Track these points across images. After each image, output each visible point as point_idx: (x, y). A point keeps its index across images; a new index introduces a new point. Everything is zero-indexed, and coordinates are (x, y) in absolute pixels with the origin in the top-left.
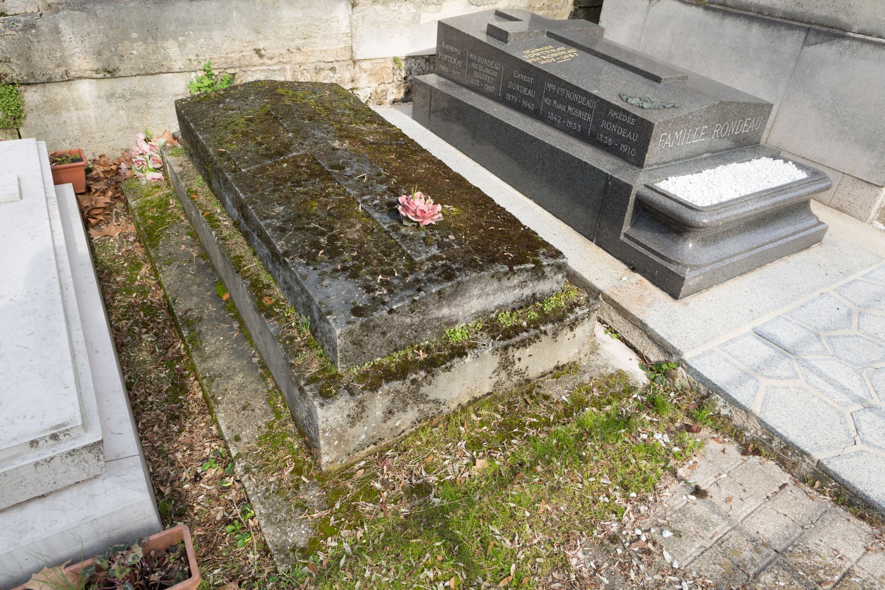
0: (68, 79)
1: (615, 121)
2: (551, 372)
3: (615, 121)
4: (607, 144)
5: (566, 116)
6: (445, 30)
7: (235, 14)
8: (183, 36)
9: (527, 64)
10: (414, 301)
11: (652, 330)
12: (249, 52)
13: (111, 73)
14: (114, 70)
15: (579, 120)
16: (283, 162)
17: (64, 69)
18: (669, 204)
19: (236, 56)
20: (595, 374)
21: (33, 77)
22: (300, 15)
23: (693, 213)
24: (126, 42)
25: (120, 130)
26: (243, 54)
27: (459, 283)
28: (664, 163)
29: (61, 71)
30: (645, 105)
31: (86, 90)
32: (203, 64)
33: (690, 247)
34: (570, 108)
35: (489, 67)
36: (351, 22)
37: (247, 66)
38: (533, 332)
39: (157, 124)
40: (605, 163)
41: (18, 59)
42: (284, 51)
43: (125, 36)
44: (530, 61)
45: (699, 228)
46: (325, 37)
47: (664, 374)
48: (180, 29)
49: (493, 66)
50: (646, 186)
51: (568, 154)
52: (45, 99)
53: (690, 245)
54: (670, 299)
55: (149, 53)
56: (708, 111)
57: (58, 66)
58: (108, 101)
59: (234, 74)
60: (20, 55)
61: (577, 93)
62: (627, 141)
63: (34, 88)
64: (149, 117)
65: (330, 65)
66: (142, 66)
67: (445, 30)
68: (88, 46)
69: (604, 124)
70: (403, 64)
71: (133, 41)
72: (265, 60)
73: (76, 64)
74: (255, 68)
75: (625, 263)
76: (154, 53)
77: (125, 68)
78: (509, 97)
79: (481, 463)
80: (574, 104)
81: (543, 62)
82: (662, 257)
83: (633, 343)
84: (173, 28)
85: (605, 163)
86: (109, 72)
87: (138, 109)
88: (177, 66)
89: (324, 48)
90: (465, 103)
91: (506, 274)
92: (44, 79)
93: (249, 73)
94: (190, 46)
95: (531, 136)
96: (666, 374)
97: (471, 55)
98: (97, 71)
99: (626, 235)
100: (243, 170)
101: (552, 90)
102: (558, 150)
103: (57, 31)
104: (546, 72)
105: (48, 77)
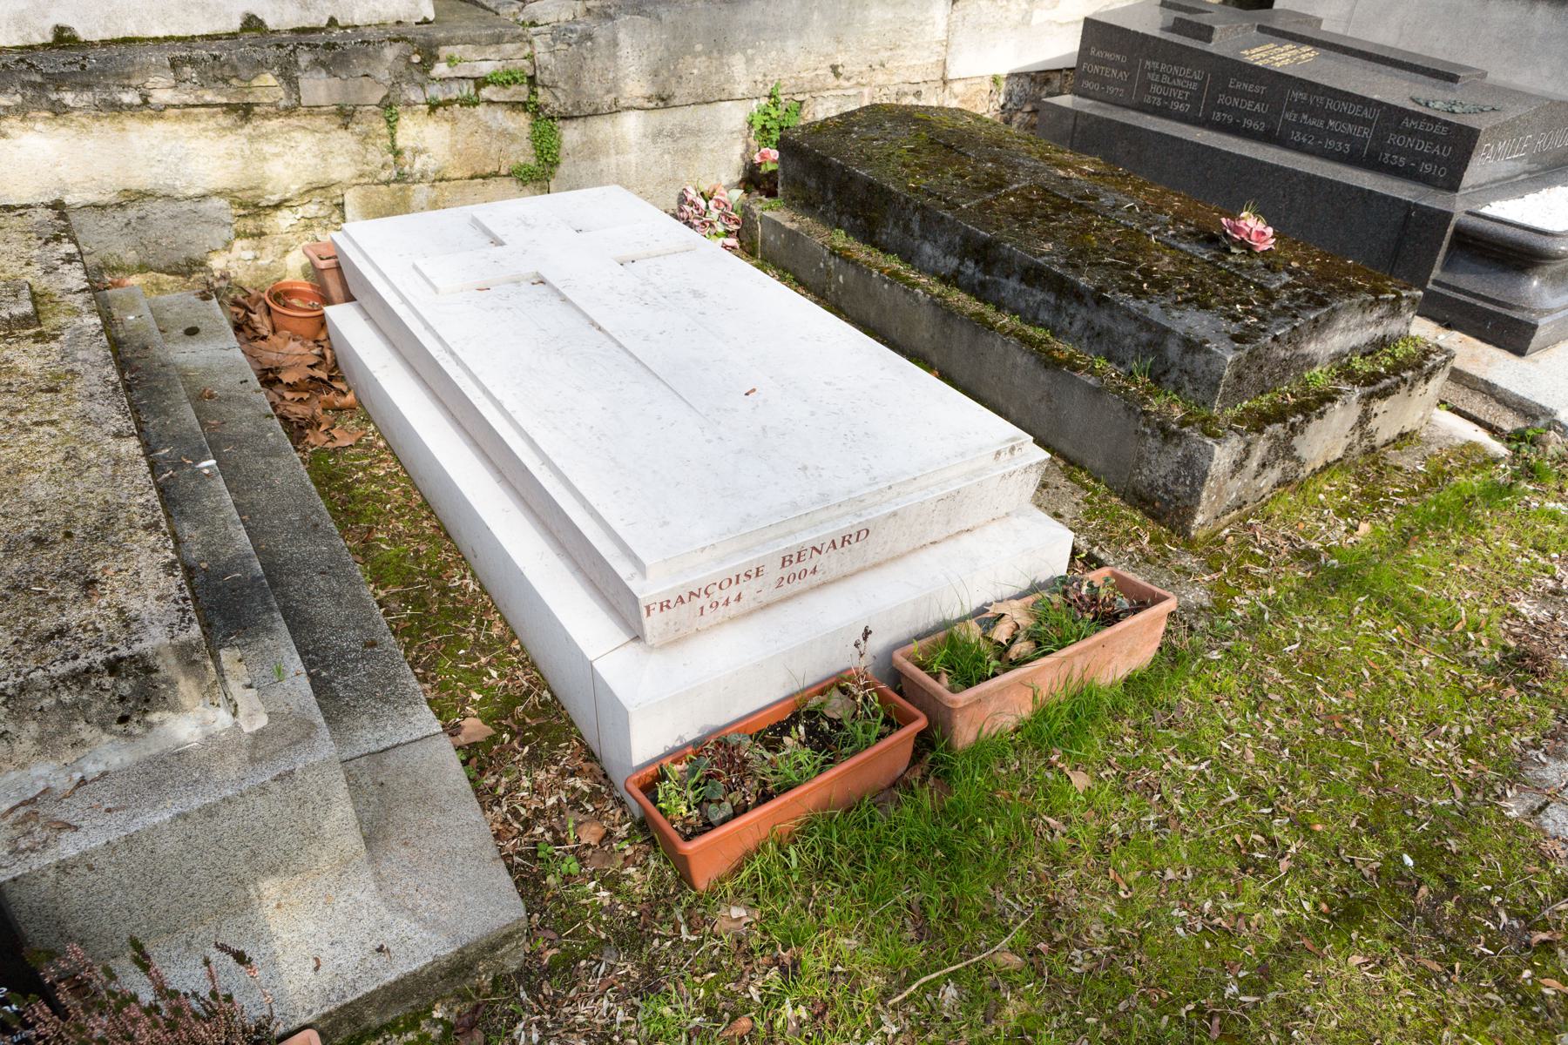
0: (615, 110)
1: (1412, 133)
2: (1394, 441)
3: (1412, 133)
4: (1397, 166)
5: (1319, 134)
6: (1095, 31)
7: (816, 16)
8: (752, 48)
9: (1256, 67)
10: (1295, 328)
11: (1505, 391)
12: (825, 70)
13: (663, 101)
14: (669, 97)
15: (1348, 138)
16: (1007, 195)
17: (613, 96)
18: (1510, 232)
19: (807, 75)
20: (1443, 444)
21: (579, 107)
22: (890, 16)
23: (1548, 239)
24: (688, 57)
25: (661, 183)
26: (818, 72)
27: (1334, 310)
28: (1480, 185)
29: (609, 98)
30: (1457, 109)
31: (631, 125)
32: (769, 87)
33: (1535, 284)
34: (1331, 123)
35: (1181, 78)
36: (948, 25)
37: (819, 90)
38: (1395, 379)
39: (705, 175)
40: (1403, 191)
41: (566, 83)
42: (864, 68)
43: (688, 49)
44: (1260, 64)
45: (1554, 259)
46: (915, 46)
47: (1531, 442)
48: (750, 38)
49: (1191, 74)
50: (1469, 213)
51: (1339, 183)
52: (585, 139)
53: (1535, 283)
54: (1512, 359)
55: (711, 73)
56: (1536, 114)
57: (609, 92)
58: (654, 142)
59: (802, 102)
60: (570, 77)
61: (1346, 101)
62: (1432, 159)
63: (574, 124)
64: (696, 165)
65: (915, 88)
66: (700, 91)
67: (1095, 31)
68: (645, 63)
69: (1393, 139)
70: (1003, 84)
71: (696, 55)
72: (842, 82)
73: (628, 89)
74: (828, 93)
75: (1434, 319)
76: (717, 72)
77: (681, 93)
78: (1217, 116)
79: (1364, 528)
80: (1339, 116)
81: (1278, 65)
82: (1498, 303)
83: (1474, 412)
84: (743, 36)
85: (1403, 191)
86: (663, 100)
87: (685, 152)
88: (740, 89)
89: (914, 62)
90: (1145, 130)
91: (1371, 303)
92: (590, 110)
93: (820, 99)
94: (759, 61)
95: (1272, 165)
96: (1533, 442)
97: (1148, 63)
98: (649, 99)
99: (1435, 282)
100: (964, 206)
101: (1299, 100)
102: (1320, 178)
103: (614, 43)
104: (1291, 77)
105: (594, 107)
